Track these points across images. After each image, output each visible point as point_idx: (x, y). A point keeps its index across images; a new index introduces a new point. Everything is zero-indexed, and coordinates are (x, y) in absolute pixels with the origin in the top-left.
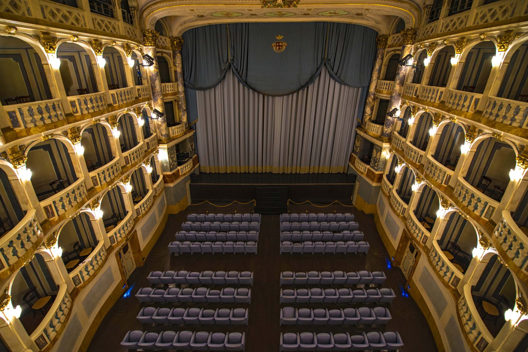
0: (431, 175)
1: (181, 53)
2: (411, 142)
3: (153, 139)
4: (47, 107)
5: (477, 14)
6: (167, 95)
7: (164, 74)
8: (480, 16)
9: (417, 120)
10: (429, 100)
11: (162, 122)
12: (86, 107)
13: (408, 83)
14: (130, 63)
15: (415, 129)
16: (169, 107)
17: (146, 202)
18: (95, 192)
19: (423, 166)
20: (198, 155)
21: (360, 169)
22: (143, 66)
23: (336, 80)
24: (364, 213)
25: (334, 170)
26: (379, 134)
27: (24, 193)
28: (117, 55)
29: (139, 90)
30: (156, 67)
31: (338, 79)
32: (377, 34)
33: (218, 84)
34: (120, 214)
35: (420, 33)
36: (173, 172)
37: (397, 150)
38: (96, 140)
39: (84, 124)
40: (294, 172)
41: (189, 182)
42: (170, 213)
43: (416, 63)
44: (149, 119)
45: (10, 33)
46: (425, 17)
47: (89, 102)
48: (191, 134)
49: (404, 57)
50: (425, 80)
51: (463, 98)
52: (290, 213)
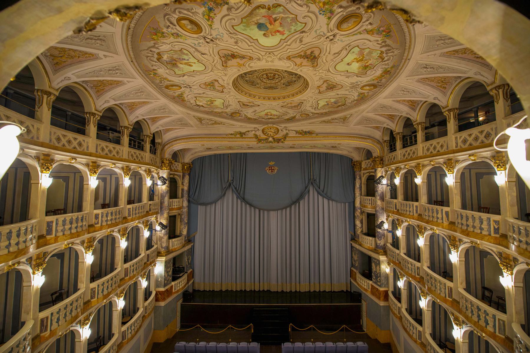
0: (433, 289)
1: (189, 175)
2: (405, 254)
3: (154, 251)
5: (423, 148)
6: (172, 209)
7: (173, 193)
8: (425, 149)
9: (405, 231)
10: (408, 213)
11: (164, 235)
13: (387, 199)
14: (149, 183)
15: (405, 240)
16: (172, 219)
17: (134, 323)
18: (90, 306)
19: (423, 278)
21: (363, 286)
22: (157, 185)
23: (323, 197)
24: (379, 342)
25: (336, 289)
26: (373, 246)
27: (30, 301)
28: (140, 177)
29: (150, 205)
30: (167, 186)
31: (325, 196)
32: (352, 160)
33: (219, 200)
34: (104, 337)
35: (386, 159)
36: (167, 288)
37: (394, 263)
38: (105, 248)
39: (99, 235)
40: (293, 290)
41: (181, 301)
42: (156, 341)
43: (389, 182)
44: (154, 231)
45: (71, 163)
46: (386, 149)
47: (110, 215)
48: (189, 247)
49: (378, 177)
50: (400, 196)
52: (293, 342)
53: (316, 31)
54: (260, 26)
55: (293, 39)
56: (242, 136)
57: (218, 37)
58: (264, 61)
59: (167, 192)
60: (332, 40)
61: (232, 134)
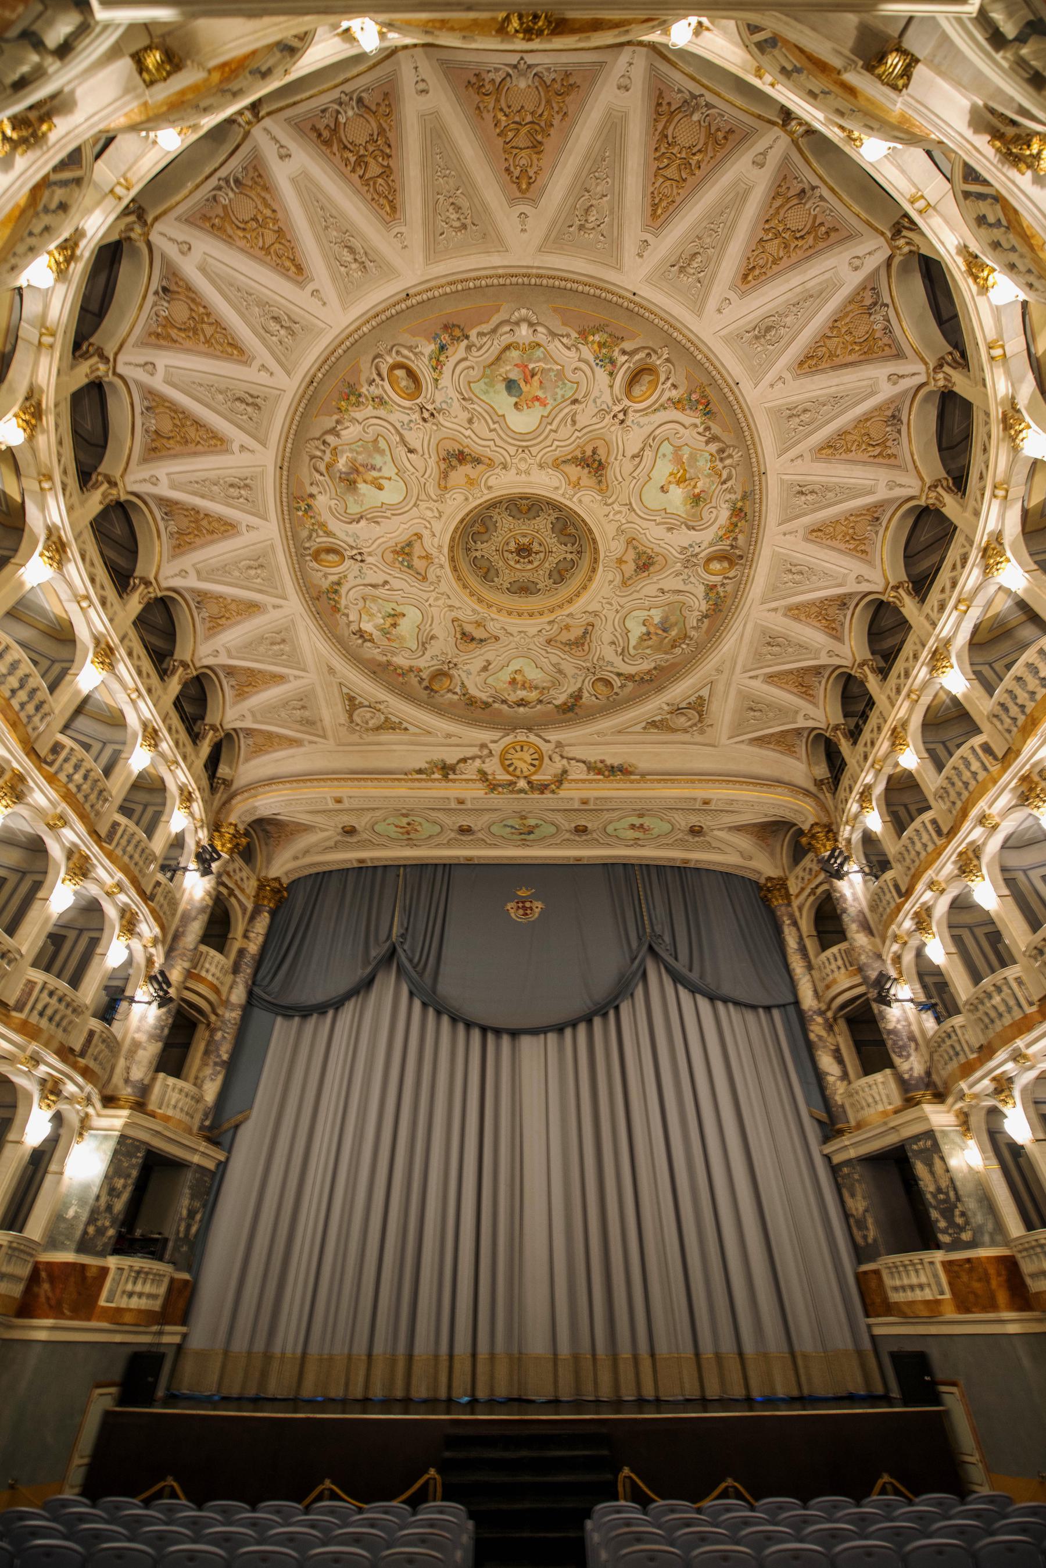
1: (273, 914)
4: (34, 691)
12: (71, 771)
20: (228, 1159)
51: (962, 767)
53: (595, 401)
54: (511, 386)
55: (561, 415)
56: (446, 776)
57: (444, 406)
58: (514, 471)
59: (202, 910)
60: (622, 422)
61: (420, 771)
